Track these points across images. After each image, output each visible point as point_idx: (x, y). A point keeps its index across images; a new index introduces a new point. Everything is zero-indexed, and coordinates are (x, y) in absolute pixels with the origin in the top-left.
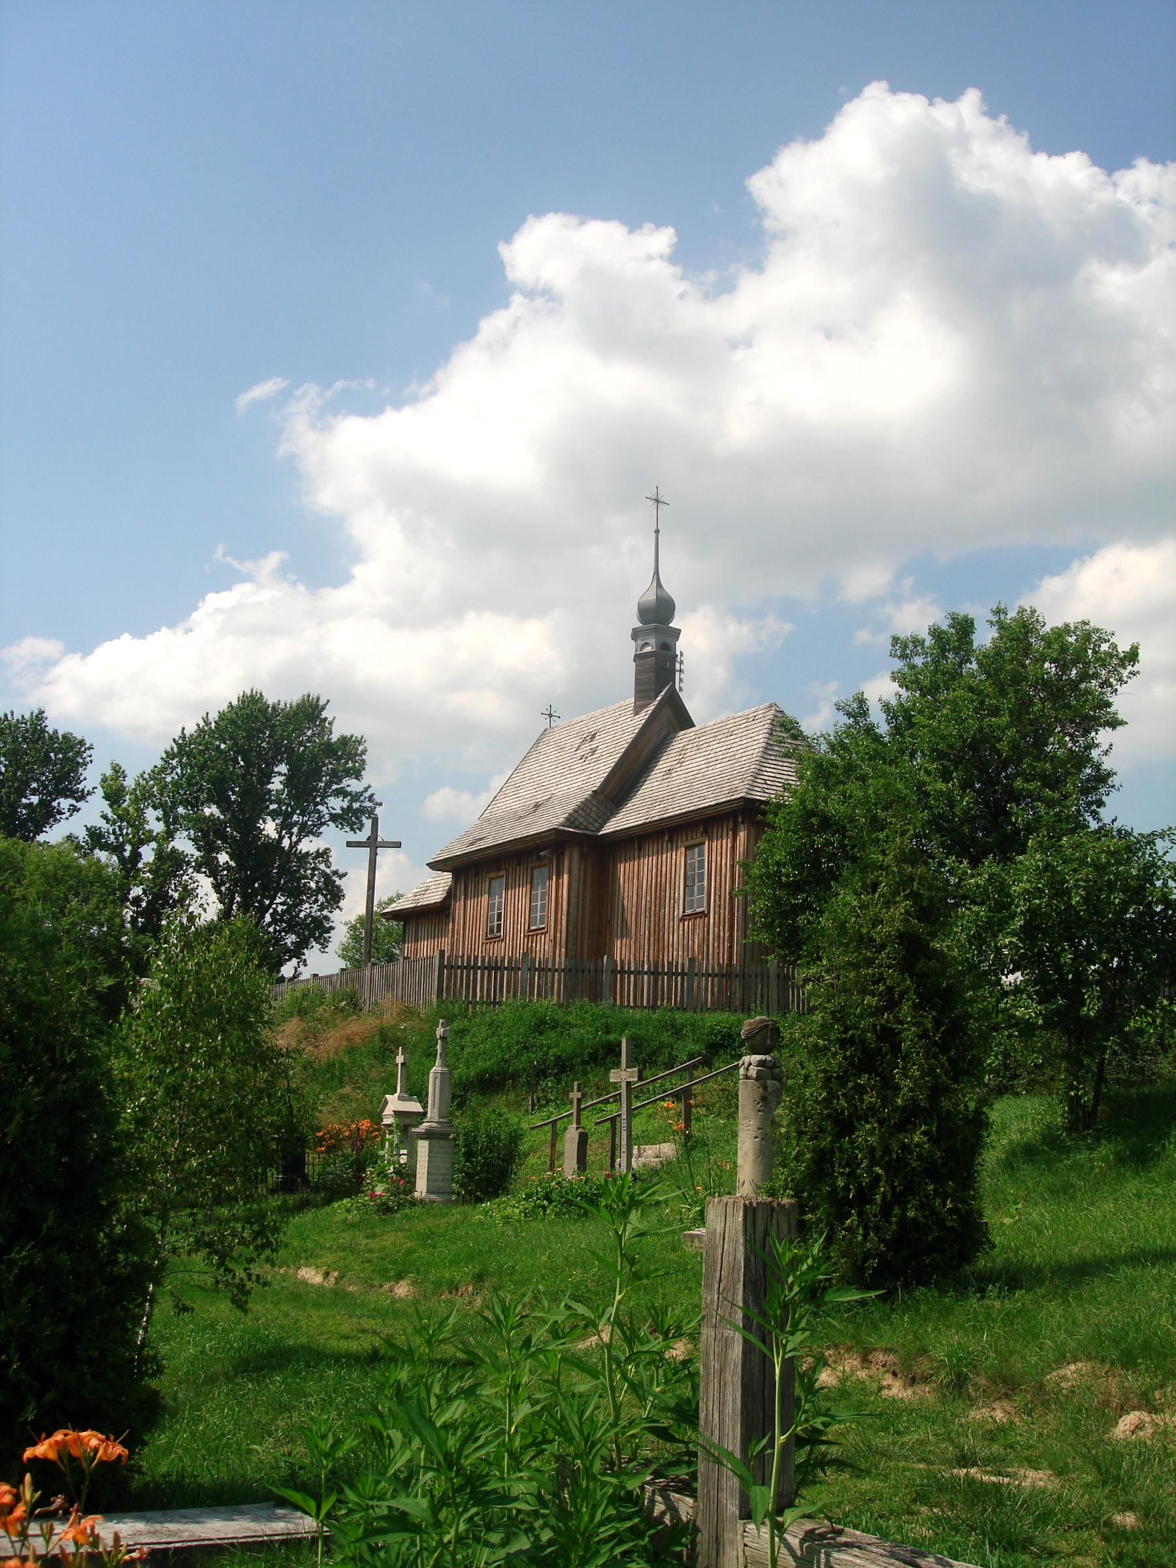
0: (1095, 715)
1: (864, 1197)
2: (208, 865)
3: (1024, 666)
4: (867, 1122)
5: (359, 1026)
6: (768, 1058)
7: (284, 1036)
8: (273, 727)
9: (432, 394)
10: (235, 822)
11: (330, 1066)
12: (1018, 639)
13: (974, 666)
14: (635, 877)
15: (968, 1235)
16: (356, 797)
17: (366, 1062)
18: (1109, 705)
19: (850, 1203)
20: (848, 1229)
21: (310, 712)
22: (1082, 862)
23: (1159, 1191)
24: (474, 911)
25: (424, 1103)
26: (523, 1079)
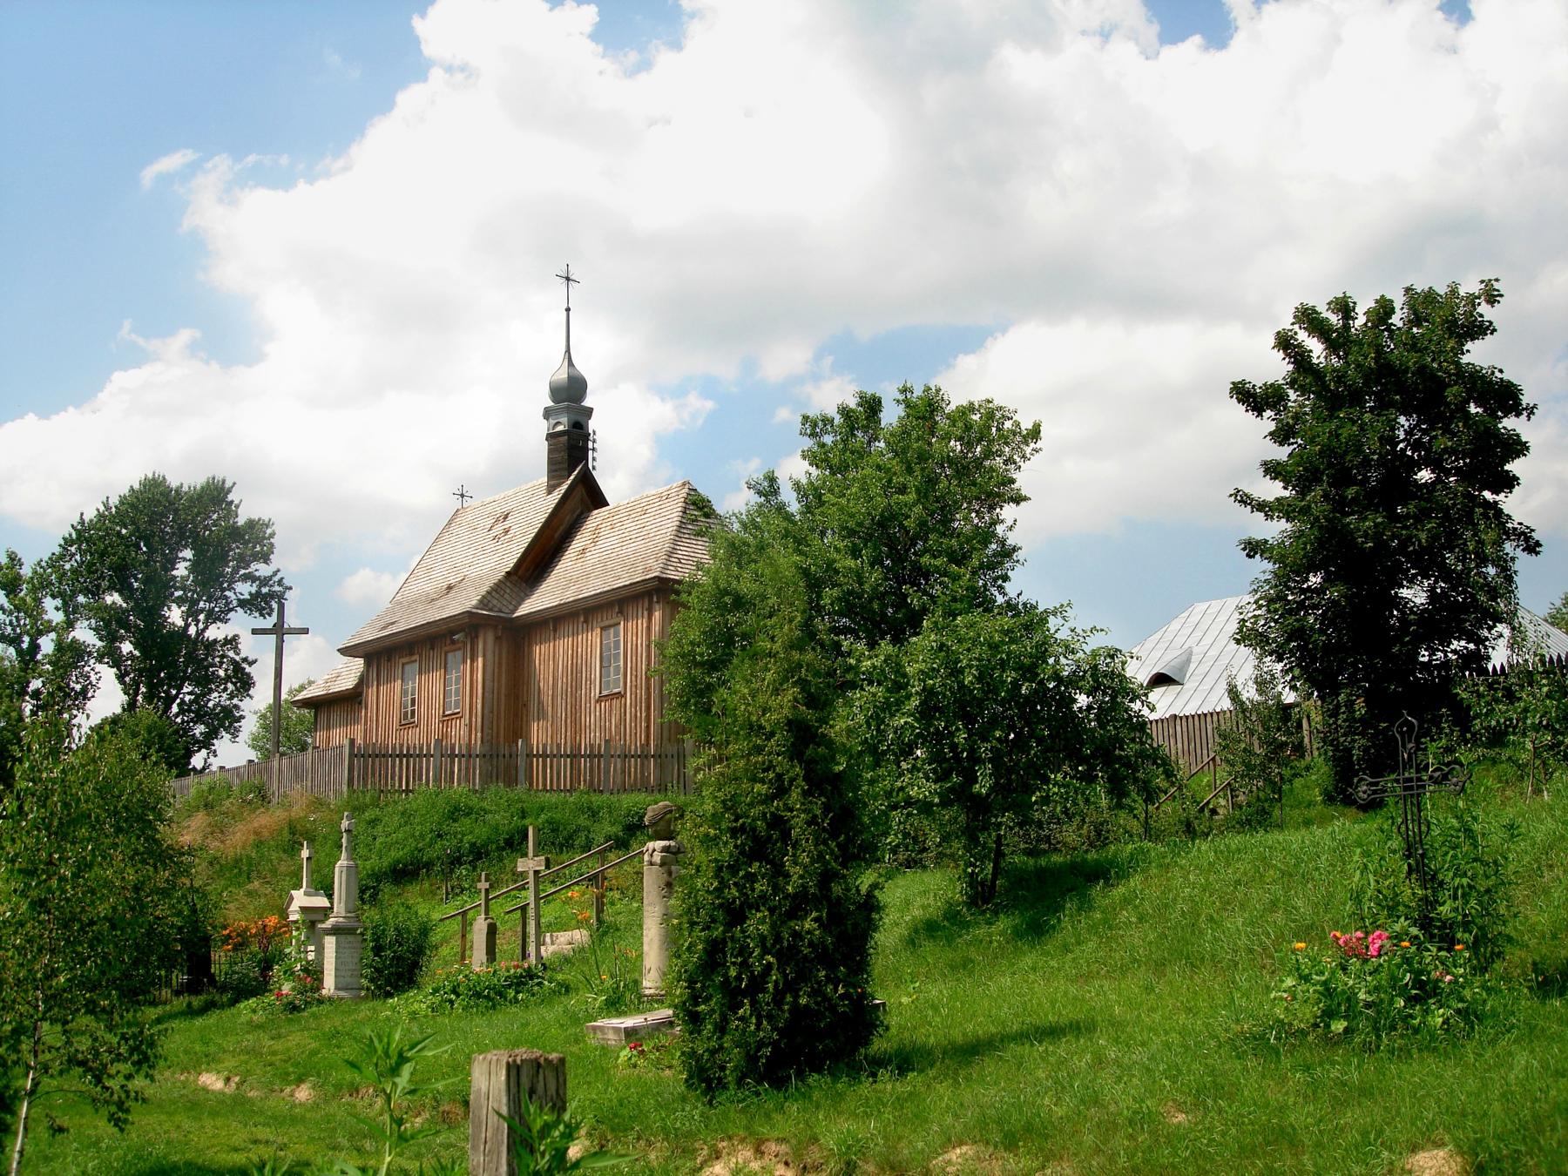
0: (1002, 492)
1: (757, 984)
2: (111, 655)
3: (930, 444)
4: (758, 910)
5: (268, 819)
6: (672, 843)
7: (187, 832)
8: (176, 511)
9: (346, 169)
10: (138, 610)
11: (238, 861)
12: (924, 418)
13: (882, 444)
14: (551, 659)
15: (862, 1019)
16: (264, 581)
17: (274, 855)
18: (1013, 481)
19: (744, 993)
20: (742, 1019)
21: (215, 495)
22: (975, 641)
23: (1053, 963)
24: (387, 698)
25: (330, 896)
26: (437, 868)
